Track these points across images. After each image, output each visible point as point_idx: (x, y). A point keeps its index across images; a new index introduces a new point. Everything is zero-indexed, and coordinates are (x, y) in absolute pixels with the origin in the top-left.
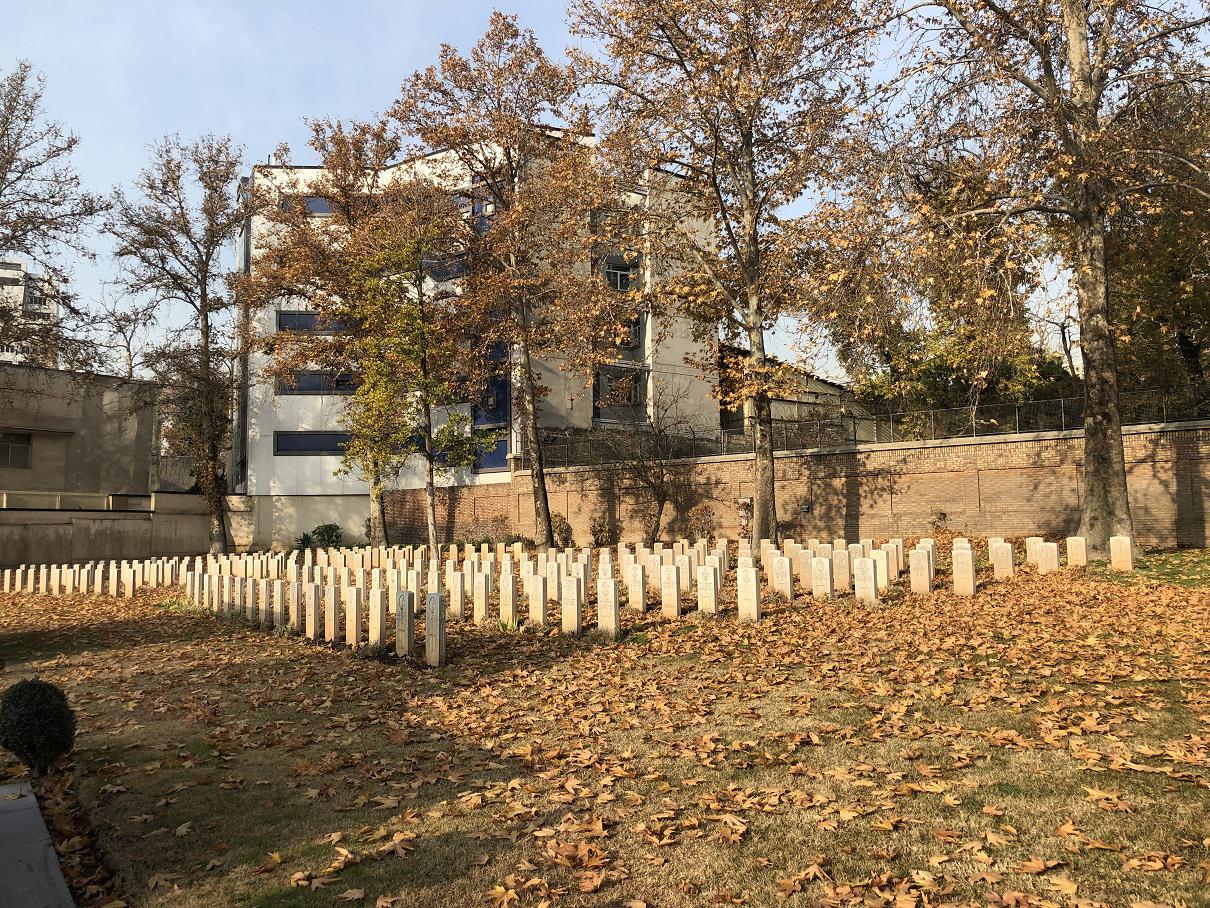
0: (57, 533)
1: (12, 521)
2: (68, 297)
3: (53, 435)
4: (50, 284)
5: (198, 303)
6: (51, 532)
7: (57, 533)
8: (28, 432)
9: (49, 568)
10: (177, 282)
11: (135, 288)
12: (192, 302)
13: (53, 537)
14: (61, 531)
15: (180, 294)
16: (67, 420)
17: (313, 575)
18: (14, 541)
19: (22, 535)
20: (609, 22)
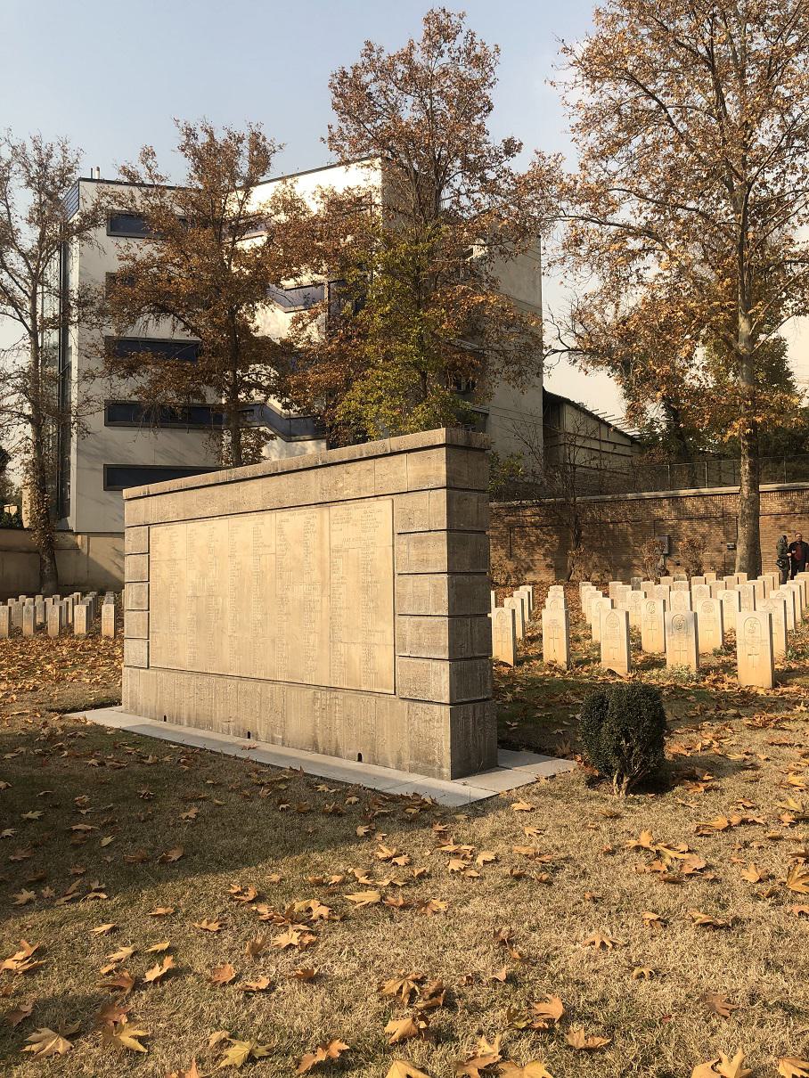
12: (22, 320)
15: (11, 310)
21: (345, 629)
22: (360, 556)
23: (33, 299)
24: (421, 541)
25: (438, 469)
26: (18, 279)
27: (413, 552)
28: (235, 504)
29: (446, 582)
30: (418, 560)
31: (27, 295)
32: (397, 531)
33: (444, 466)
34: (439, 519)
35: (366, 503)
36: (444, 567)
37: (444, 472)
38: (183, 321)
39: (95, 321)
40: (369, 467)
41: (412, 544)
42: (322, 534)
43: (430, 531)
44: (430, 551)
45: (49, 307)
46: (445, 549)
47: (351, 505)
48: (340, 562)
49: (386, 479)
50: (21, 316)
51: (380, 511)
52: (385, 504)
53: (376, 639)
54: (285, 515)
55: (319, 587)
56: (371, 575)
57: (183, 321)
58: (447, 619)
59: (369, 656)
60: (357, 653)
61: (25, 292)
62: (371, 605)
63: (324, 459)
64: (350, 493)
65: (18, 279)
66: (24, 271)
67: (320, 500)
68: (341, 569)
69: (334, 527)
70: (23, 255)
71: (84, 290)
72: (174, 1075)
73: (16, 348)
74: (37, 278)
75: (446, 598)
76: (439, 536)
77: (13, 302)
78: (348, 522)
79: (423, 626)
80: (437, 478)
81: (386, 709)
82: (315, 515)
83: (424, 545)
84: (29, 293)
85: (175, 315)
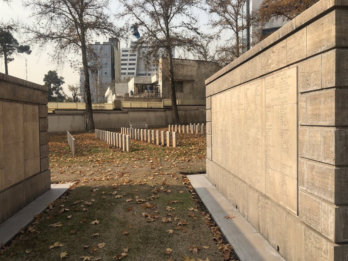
0: (194, 113)
1: (182, 109)
2: (196, 29)
3: (189, 81)
4: (190, 25)
5: (235, 29)
6: (193, 112)
7: (194, 113)
8: (181, 81)
9: (178, 126)
10: (228, 21)
11: (215, 25)
12: (233, 29)
13: (193, 114)
14: (196, 112)
15: (229, 26)
16: (192, 76)
17: (345, 126)
18: (183, 115)
19: (185, 113)
20: (90, 143)
21: (272, 160)
22: (280, 110)
23: (236, 21)
24: (315, 99)
25: (329, 32)
26: (231, 15)
27: (309, 107)
28: (232, 82)
29: (334, 134)
30: (313, 114)
31: (234, 20)
32: (301, 90)
33: (334, 28)
34: (329, 78)
35: (281, 72)
36: (331, 120)
37: (333, 34)
38: (287, 17)
39: (256, 24)
40: (284, 45)
41: (309, 101)
42: (262, 97)
43: (322, 89)
44: (322, 106)
45: (241, 22)
46: (333, 105)
47: (275, 74)
48: (270, 114)
49: (293, 51)
50: (232, 27)
51: (289, 77)
52: (292, 71)
53: (287, 171)
54: (247, 86)
55: (260, 130)
56: (285, 125)
57: (287, 17)
58: (334, 167)
59: (283, 183)
60: (277, 177)
61: (234, 19)
62: (285, 146)
63: (262, 46)
64: (274, 67)
65: (231, 15)
66: (233, 12)
67: (261, 74)
68: (270, 119)
69: (267, 91)
70: (233, 6)
71: (253, 12)
72: (347, 218)
73: (231, 39)
74: (237, 13)
75: (333, 149)
76: (328, 93)
77: (231, 24)
78: (273, 87)
79: (316, 170)
80: (328, 40)
81: (292, 224)
82: (259, 84)
83: (317, 101)
84: (235, 19)
85: (284, 15)
